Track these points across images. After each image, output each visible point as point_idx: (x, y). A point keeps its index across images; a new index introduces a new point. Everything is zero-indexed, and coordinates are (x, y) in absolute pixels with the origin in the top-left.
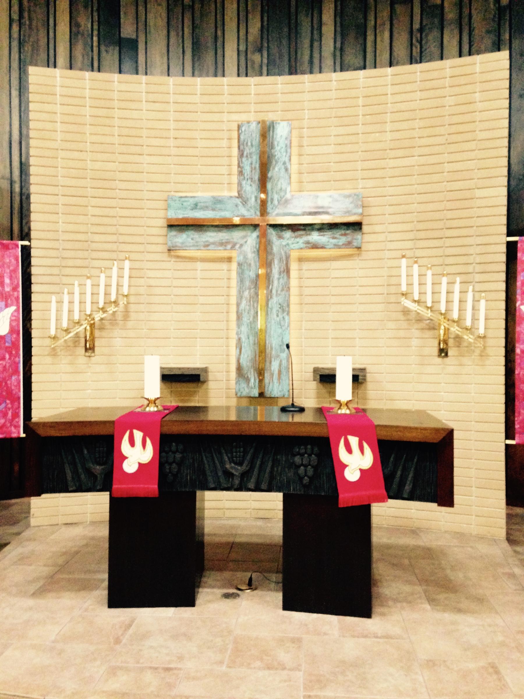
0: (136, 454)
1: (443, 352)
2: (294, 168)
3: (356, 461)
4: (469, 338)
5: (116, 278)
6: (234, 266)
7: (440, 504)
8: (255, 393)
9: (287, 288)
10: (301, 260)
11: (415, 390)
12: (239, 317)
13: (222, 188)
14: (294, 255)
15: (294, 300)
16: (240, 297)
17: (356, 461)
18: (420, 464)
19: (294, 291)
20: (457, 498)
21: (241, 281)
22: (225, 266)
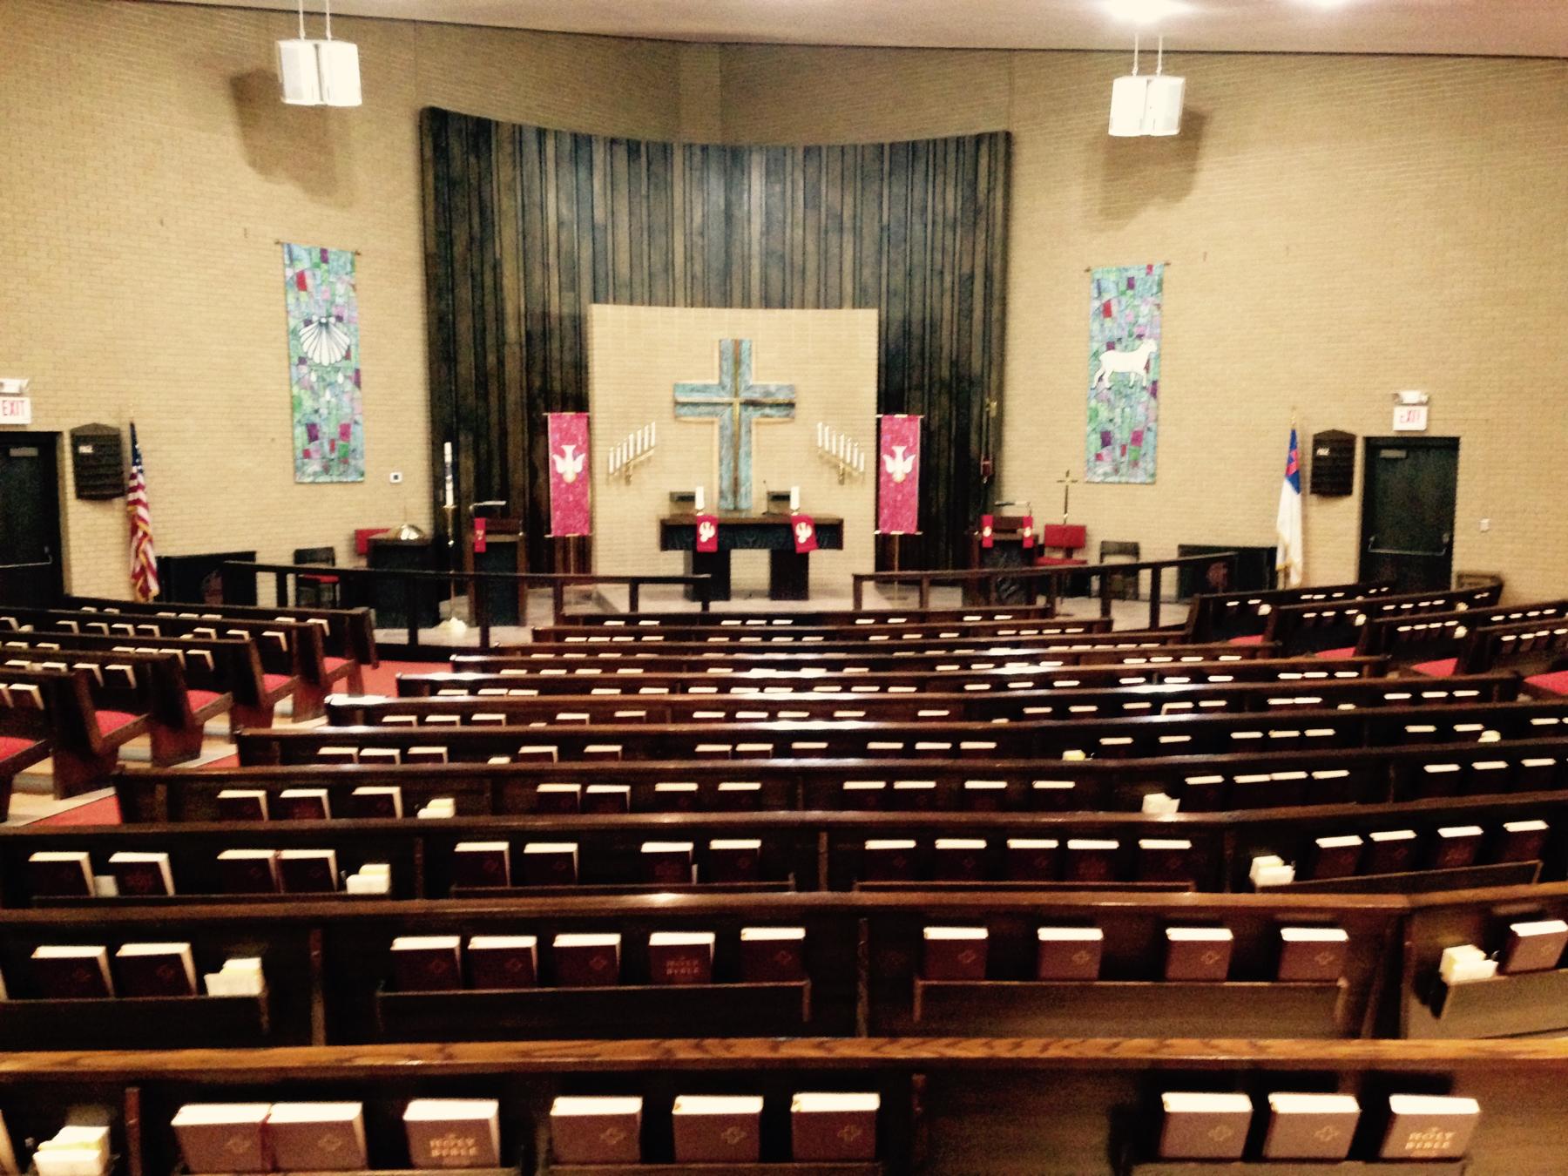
0: (707, 533)
1: (842, 482)
2: (753, 366)
3: (804, 533)
4: (855, 474)
5: (646, 435)
6: (716, 428)
7: (49, 1137)
8: (731, 507)
9: (749, 442)
10: (758, 423)
11: (811, 499)
12: (721, 460)
13: (706, 373)
14: (754, 420)
15: (754, 448)
16: (721, 447)
17: (804, 533)
18: (830, 534)
19: (754, 443)
20: (846, 544)
21: (722, 437)
22: (709, 427)
